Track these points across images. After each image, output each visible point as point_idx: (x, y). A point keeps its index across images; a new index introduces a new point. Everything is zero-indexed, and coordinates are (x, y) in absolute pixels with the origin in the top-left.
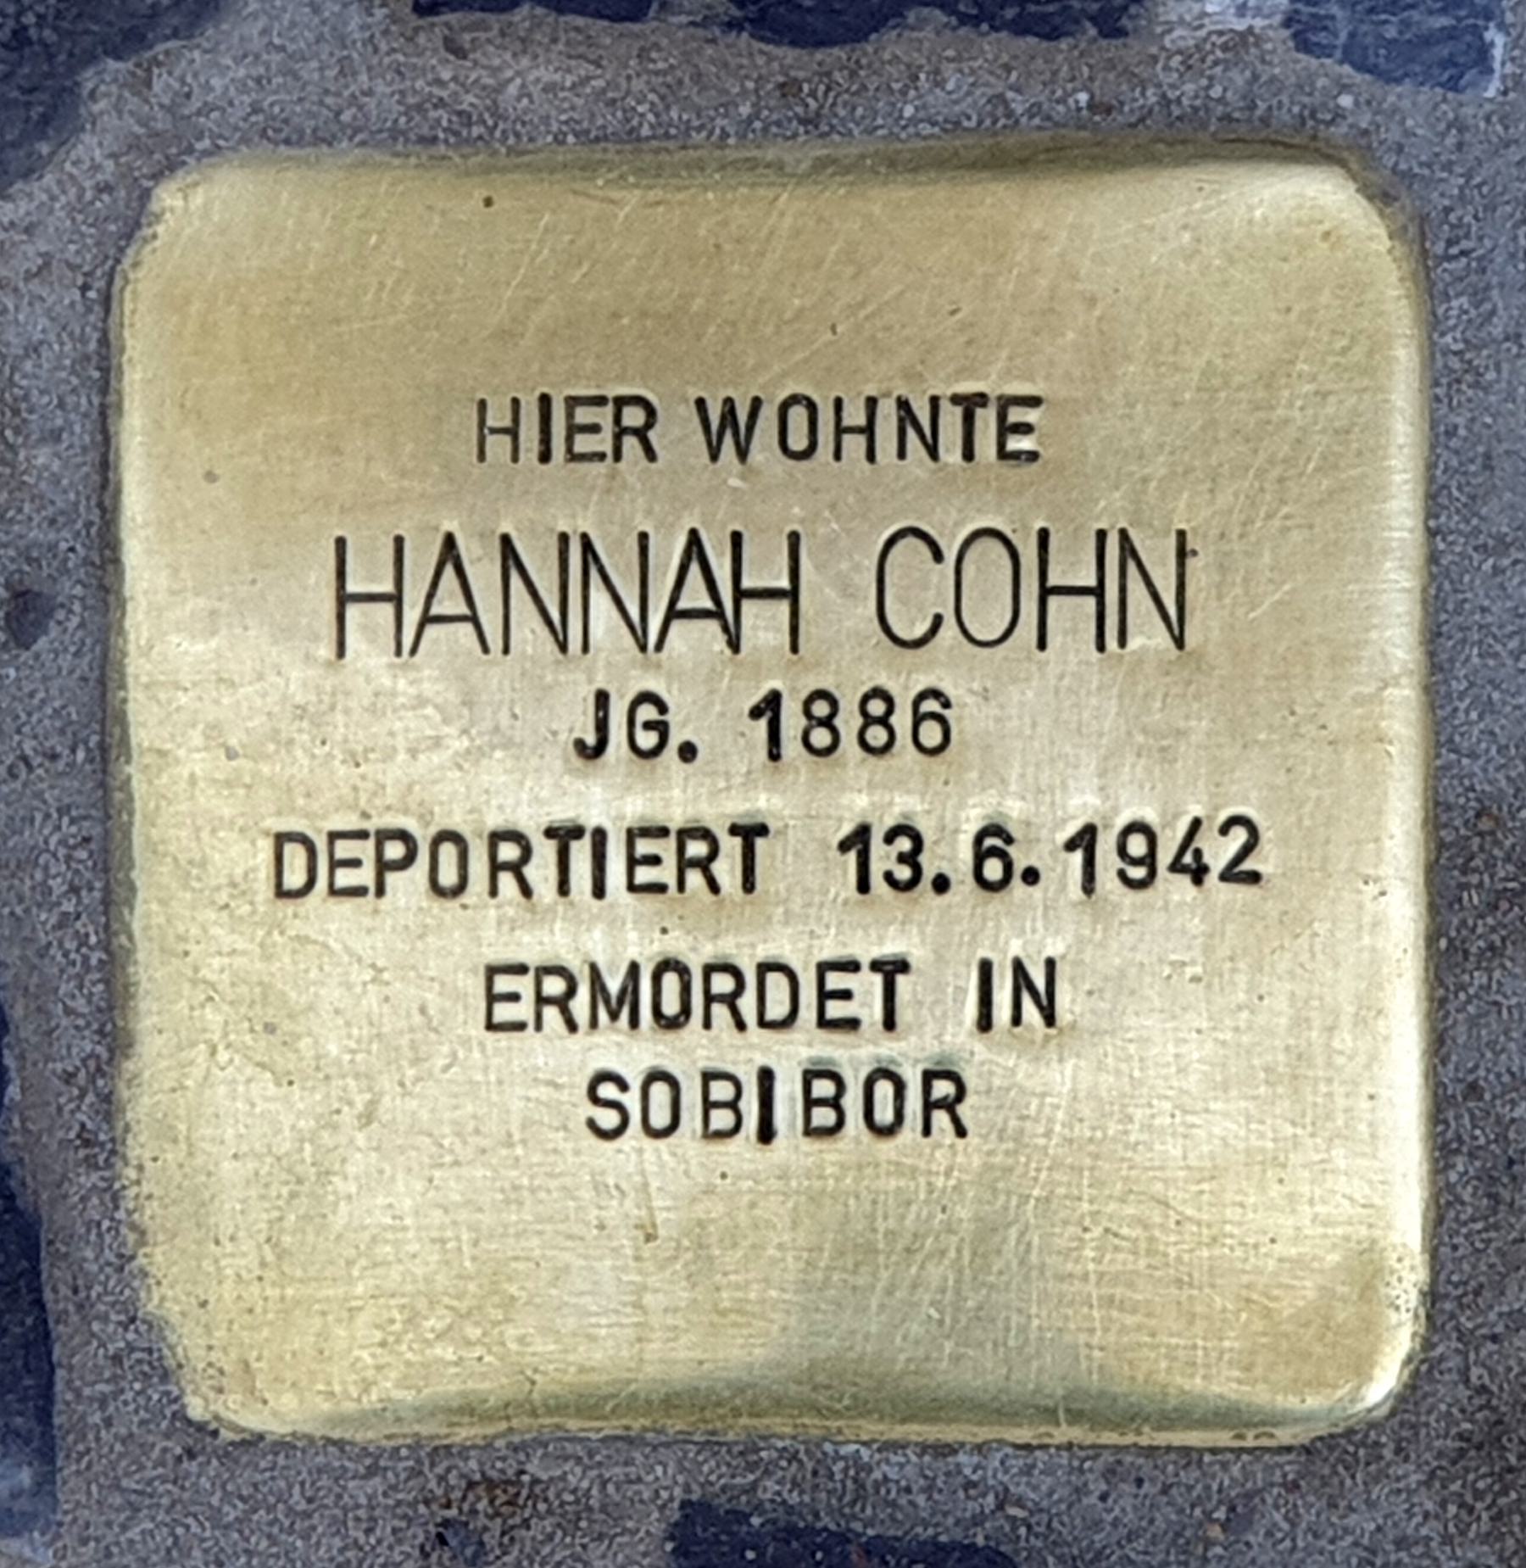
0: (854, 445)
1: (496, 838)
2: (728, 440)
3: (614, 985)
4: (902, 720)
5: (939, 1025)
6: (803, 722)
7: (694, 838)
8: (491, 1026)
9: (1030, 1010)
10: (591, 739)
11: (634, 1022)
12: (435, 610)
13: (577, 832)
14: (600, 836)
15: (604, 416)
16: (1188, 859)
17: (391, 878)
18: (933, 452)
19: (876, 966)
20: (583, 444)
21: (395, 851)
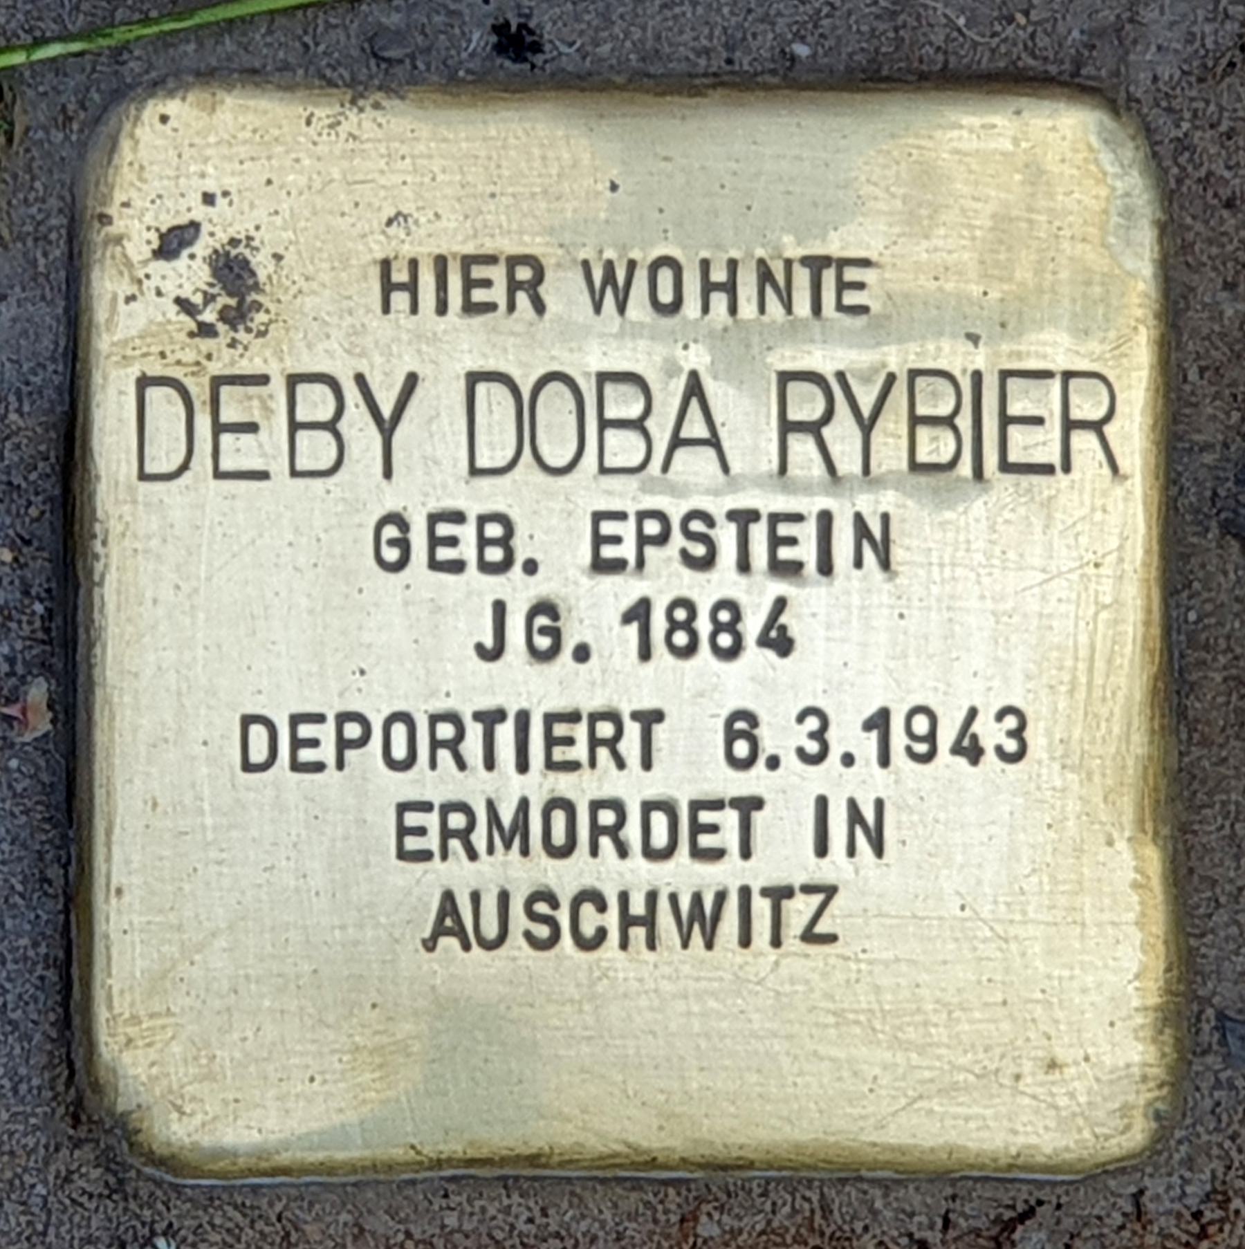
0: (719, 301)
1: (434, 719)
2: (609, 293)
3: (507, 817)
4: (704, 626)
5: (783, 851)
8: (402, 855)
9: (869, 556)
10: (489, 642)
11: (525, 852)
12: (684, 434)
13: (500, 715)
14: (523, 720)
17: (350, 755)
18: (789, 309)
21: (353, 731)
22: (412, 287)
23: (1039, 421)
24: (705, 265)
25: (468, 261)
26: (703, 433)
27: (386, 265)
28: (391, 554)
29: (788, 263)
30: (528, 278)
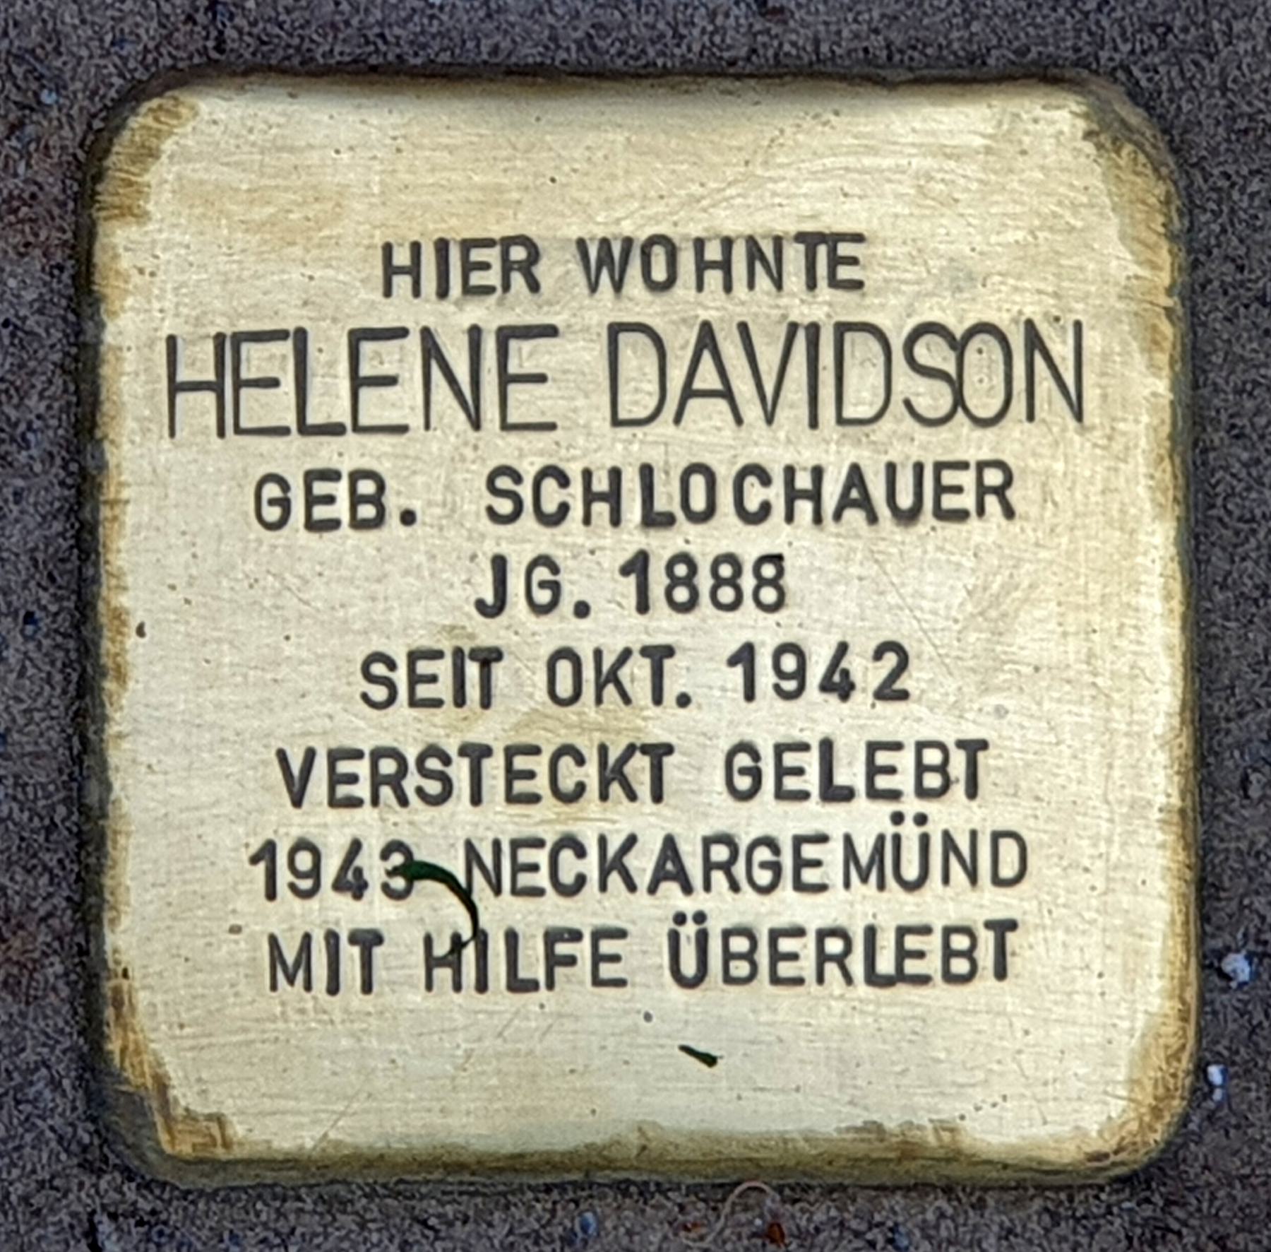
0: (714, 278)
2: (605, 277)
4: (704, 582)
6: (667, 581)
7: (367, 339)
10: (489, 598)
12: (698, 385)
15: (492, 255)
16: (837, 678)
18: (778, 284)
19: (645, 651)
20: (477, 278)
22: (414, 269)
23: (274, 383)
24: (699, 244)
25: (467, 245)
26: (717, 385)
27: (388, 249)
28: (272, 514)
29: (778, 242)
30: (522, 257)
